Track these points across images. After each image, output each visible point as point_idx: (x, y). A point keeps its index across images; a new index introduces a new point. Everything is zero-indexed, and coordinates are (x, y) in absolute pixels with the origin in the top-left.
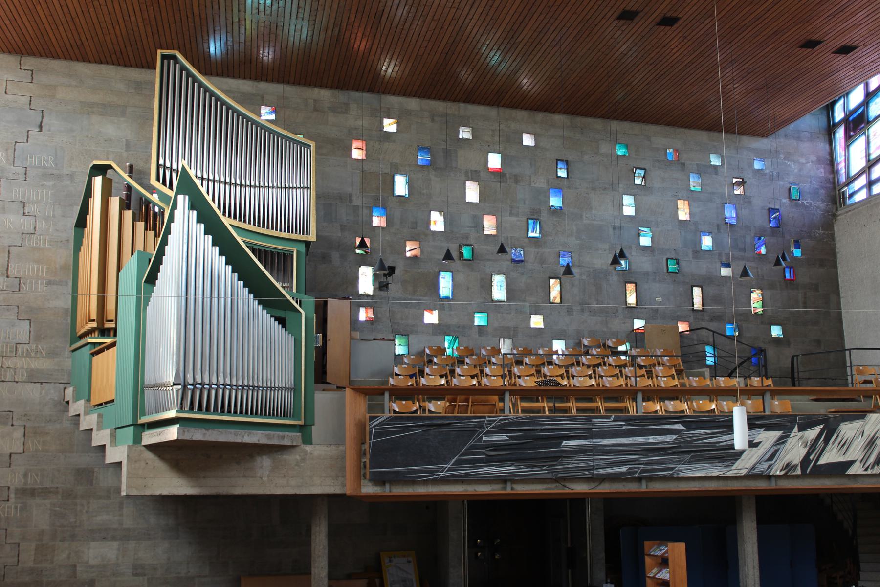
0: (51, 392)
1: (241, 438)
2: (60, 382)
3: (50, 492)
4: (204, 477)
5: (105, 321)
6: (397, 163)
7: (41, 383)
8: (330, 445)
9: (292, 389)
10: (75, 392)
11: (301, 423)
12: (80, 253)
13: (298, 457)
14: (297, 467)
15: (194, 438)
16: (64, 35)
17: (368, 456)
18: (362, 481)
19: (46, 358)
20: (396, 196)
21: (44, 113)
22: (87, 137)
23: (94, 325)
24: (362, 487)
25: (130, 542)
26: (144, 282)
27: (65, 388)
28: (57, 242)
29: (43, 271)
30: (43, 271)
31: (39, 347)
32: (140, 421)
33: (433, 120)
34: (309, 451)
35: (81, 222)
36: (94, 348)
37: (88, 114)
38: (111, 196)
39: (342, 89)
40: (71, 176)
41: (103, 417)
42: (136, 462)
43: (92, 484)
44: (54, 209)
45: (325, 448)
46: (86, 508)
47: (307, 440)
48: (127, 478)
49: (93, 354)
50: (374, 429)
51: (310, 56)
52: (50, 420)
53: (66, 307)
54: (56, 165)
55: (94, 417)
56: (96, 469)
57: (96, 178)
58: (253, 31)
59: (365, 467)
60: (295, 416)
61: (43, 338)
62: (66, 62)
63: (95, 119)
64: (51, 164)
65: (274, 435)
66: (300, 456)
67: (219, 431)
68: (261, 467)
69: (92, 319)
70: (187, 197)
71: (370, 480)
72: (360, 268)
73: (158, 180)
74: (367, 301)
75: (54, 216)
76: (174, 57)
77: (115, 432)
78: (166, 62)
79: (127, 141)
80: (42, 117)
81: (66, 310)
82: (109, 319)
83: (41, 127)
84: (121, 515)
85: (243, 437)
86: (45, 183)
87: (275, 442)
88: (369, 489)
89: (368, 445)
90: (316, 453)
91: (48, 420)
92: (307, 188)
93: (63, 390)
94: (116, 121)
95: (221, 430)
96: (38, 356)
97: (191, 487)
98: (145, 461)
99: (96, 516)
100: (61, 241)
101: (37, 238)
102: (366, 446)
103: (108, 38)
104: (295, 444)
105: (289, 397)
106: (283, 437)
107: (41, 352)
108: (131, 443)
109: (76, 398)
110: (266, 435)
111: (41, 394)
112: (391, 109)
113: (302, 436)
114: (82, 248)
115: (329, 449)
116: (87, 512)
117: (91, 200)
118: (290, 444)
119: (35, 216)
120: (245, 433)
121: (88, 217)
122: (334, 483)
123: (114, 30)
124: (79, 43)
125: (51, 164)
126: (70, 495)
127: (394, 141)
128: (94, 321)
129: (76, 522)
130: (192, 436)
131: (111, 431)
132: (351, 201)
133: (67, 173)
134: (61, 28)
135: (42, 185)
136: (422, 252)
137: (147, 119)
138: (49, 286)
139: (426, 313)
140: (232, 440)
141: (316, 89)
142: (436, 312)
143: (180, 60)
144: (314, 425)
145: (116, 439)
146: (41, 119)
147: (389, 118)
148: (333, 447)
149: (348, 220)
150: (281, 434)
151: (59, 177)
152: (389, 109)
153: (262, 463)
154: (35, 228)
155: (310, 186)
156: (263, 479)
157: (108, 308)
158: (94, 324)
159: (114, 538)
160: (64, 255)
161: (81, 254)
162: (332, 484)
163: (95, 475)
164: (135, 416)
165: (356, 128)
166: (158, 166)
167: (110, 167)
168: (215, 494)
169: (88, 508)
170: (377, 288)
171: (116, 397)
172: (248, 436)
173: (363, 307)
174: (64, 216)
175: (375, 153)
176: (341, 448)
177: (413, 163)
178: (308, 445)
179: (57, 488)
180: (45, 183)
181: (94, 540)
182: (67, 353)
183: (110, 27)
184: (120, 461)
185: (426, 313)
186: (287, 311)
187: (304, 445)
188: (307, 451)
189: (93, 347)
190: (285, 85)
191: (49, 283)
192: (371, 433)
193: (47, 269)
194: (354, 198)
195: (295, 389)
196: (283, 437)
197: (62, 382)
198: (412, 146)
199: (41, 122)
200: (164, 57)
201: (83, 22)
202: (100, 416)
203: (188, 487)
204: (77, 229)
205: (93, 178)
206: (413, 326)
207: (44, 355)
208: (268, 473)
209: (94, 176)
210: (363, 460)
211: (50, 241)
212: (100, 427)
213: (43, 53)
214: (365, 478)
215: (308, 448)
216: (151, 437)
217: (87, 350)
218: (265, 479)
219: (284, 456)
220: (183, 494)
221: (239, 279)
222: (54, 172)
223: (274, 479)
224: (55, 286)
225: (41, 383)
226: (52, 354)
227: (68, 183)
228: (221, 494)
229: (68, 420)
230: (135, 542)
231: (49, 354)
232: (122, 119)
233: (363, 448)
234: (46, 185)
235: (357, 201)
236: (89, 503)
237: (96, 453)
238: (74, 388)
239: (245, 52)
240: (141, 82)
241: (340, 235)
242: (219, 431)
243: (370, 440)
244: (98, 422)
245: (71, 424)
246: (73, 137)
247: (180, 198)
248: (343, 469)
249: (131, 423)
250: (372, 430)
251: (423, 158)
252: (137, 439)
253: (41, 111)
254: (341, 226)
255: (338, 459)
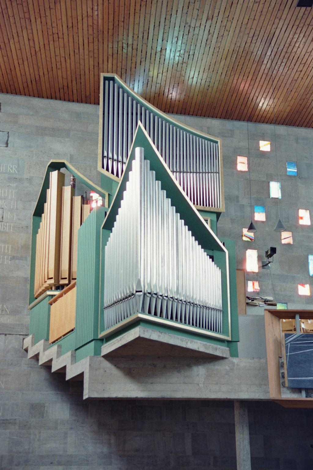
0: (13, 342)
1: (185, 343)
2: (20, 334)
3: (9, 423)
4: (152, 383)
5: (60, 279)
6: (271, 174)
7: (6, 335)
8: (253, 358)
9: (221, 311)
10: (33, 339)
11: (229, 339)
12: (38, 235)
13: (227, 368)
14: (227, 376)
15: (152, 338)
16: (27, 69)
17: (285, 366)
18: (282, 389)
19: (9, 315)
20: (272, 198)
21: (9, 134)
22: (41, 152)
23: (52, 281)
24: (282, 394)
25: (72, 467)
26: (103, 228)
27: (24, 339)
28: (19, 228)
29: (8, 249)
30: (8, 249)
31: (5, 306)
32: (101, 335)
33: (297, 142)
34: (236, 363)
35: (39, 212)
36: (52, 298)
37: (42, 135)
38: (64, 186)
39: (228, 119)
40: (30, 180)
41: (62, 347)
42: (96, 370)
43: (43, 417)
44: (17, 203)
45: (249, 360)
46: (38, 437)
47: (234, 354)
48: (89, 383)
49: (51, 304)
50: (289, 344)
51: (209, 86)
52: (12, 364)
53: (25, 276)
54: (18, 171)
55: (55, 348)
56: (47, 404)
57: (53, 172)
58: (170, 61)
59: (283, 377)
60: (225, 332)
61: (8, 300)
62: (25, 98)
63: (47, 139)
64: (14, 170)
65: (209, 346)
66: (229, 366)
67: (170, 336)
68: (198, 375)
69: (50, 277)
70: (143, 149)
71: (288, 388)
72: (247, 251)
73: (103, 167)
74: (254, 277)
75: (17, 209)
76: (113, 79)
77: (75, 353)
78: (107, 82)
79: (70, 155)
80: (8, 137)
81: (26, 279)
82: (63, 277)
83: (7, 144)
84: (66, 443)
85: (187, 343)
86: (10, 184)
87: (210, 351)
88: (288, 395)
89: (285, 357)
90: (242, 365)
91: (10, 364)
92: (216, 173)
93: (22, 341)
94: (63, 141)
95: (171, 335)
96: (3, 314)
97: (141, 391)
98: (104, 369)
99: (45, 444)
100: (22, 227)
101: (4, 225)
102: (284, 360)
103: (60, 72)
104: (224, 356)
105: (220, 316)
106: (216, 349)
107: (6, 311)
108: (93, 354)
109: (34, 342)
110: (204, 345)
111: (5, 343)
112: (265, 134)
113: (230, 350)
114: (39, 230)
115: (253, 361)
116: (38, 440)
117: (48, 191)
118: (221, 355)
119: (3, 208)
120: (188, 341)
121: (46, 205)
122: (258, 390)
123: (66, 64)
124: (37, 77)
125: (14, 170)
126: (25, 426)
127: (268, 158)
128: (52, 278)
129: (29, 449)
130: (150, 336)
131: (72, 352)
132: (238, 201)
133: (27, 177)
134: (26, 63)
135: (8, 186)
136: (294, 240)
137: (86, 140)
138: (13, 260)
139: (300, 287)
140: (179, 345)
141: (209, 119)
142: (307, 286)
143: (117, 80)
144: (239, 341)
145: (75, 359)
146: (7, 138)
147: (264, 141)
148: (256, 360)
149: (236, 215)
150: (215, 346)
151: (21, 180)
152: (264, 134)
153: (198, 372)
154: (3, 217)
155: (219, 171)
156: (200, 385)
157: (62, 269)
158: (52, 281)
159: (59, 464)
160: (24, 238)
161: (38, 236)
162: (256, 391)
163: (46, 409)
164: (96, 332)
165: (240, 148)
166: (103, 157)
167: (63, 165)
168: (160, 397)
169: (40, 436)
170: (260, 267)
171: (77, 326)
172: (191, 343)
173: (250, 281)
174: (24, 209)
175: (255, 166)
176: (263, 361)
177: (284, 173)
178: (235, 358)
179: (15, 420)
180: (10, 184)
181: (43, 464)
182: (26, 311)
183: (63, 60)
184: (81, 372)
185: (300, 287)
186: (214, 251)
187: (232, 358)
188: (234, 362)
189: (51, 297)
190: (186, 117)
191: (13, 258)
192: (287, 347)
193: (12, 247)
194: (240, 199)
195: (224, 311)
196: (216, 349)
197: (22, 334)
198: (282, 161)
199: (8, 140)
200: (105, 79)
201: (43, 56)
202: (59, 347)
203: (139, 391)
204: (35, 217)
205: (51, 172)
206: (290, 296)
207: (9, 313)
208: (203, 380)
209: (52, 171)
210: (281, 371)
211: (14, 227)
212: (59, 354)
213: (9, 91)
214: (284, 386)
215: (235, 360)
216: (108, 348)
217: (47, 301)
218: (201, 385)
219: (216, 367)
220: (135, 397)
221: (181, 219)
222: (17, 176)
223: (209, 386)
224: (17, 261)
225: (6, 335)
226: (15, 312)
227: (28, 185)
228: (166, 397)
229: (25, 364)
230: (76, 467)
231: (12, 312)
232: (67, 139)
233: (281, 362)
234: (11, 186)
235: (244, 201)
236: (40, 433)
237: (47, 391)
238: (33, 335)
239: (161, 84)
240: (80, 113)
241: (231, 226)
242: (170, 336)
243: (287, 353)
244: (57, 352)
245: (28, 367)
246: (32, 151)
247: (138, 150)
248: (265, 378)
249: (92, 339)
250: (288, 345)
251: (292, 170)
252: (97, 352)
253: (7, 133)
254: (231, 219)
255: (260, 370)
